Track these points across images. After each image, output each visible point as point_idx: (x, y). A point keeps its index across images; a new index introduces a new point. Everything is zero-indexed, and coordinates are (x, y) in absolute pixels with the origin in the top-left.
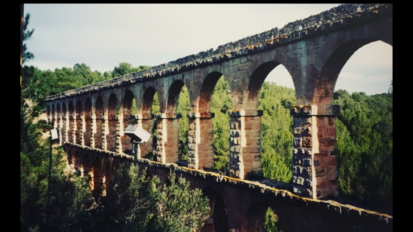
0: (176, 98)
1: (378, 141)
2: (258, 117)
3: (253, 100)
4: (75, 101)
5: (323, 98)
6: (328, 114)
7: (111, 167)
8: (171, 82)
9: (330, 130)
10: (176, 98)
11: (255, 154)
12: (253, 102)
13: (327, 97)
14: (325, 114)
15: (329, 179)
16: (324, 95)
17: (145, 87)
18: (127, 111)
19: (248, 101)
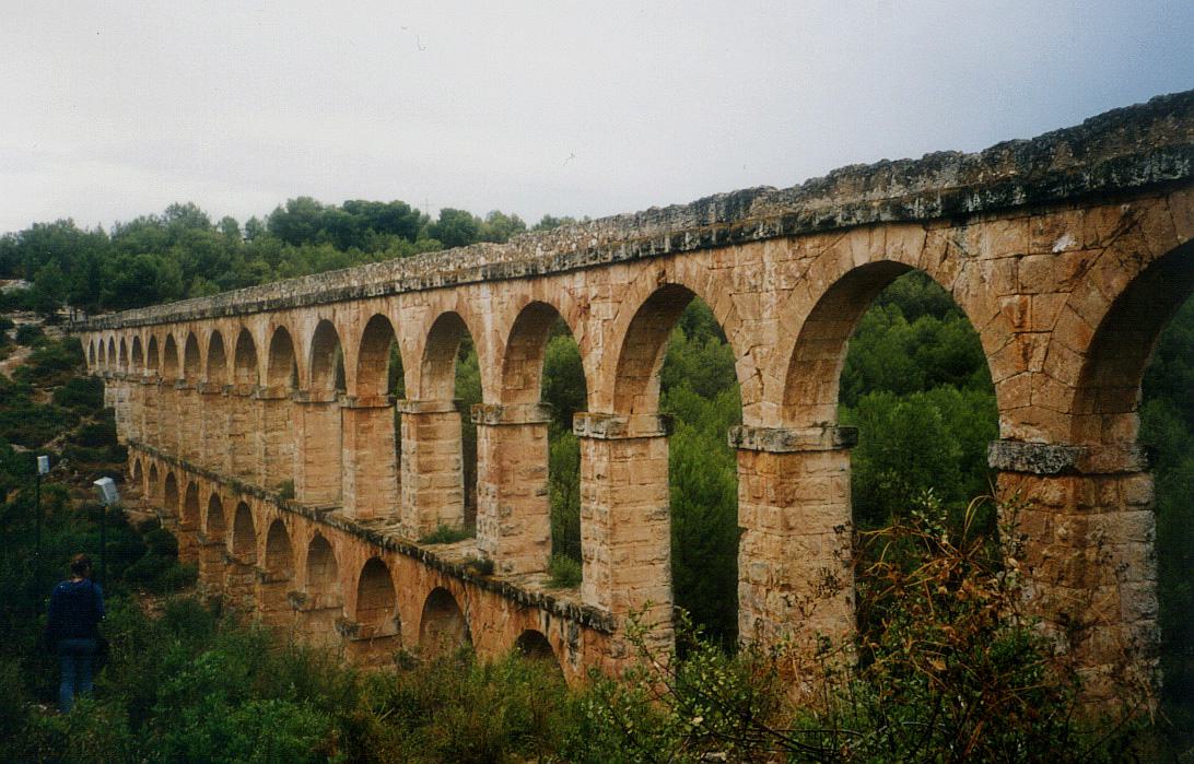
0: (330, 355)
1: (263, 472)
2: (454, 414)
3: (443, 380)
4: (144, 338)
5: (519, 393)
6: (529, 421)
7: (88, 355)
8: (316, 322)
9: (535, 450)
10: (330, 355)
11: (448, 491)
12: (443, 384)
13: (528, 389)
14: (523, 422)
15: (531, 539)
16: (521, 387)
17: (273, 324)
18: (246, 374)
19: (431, 382)
